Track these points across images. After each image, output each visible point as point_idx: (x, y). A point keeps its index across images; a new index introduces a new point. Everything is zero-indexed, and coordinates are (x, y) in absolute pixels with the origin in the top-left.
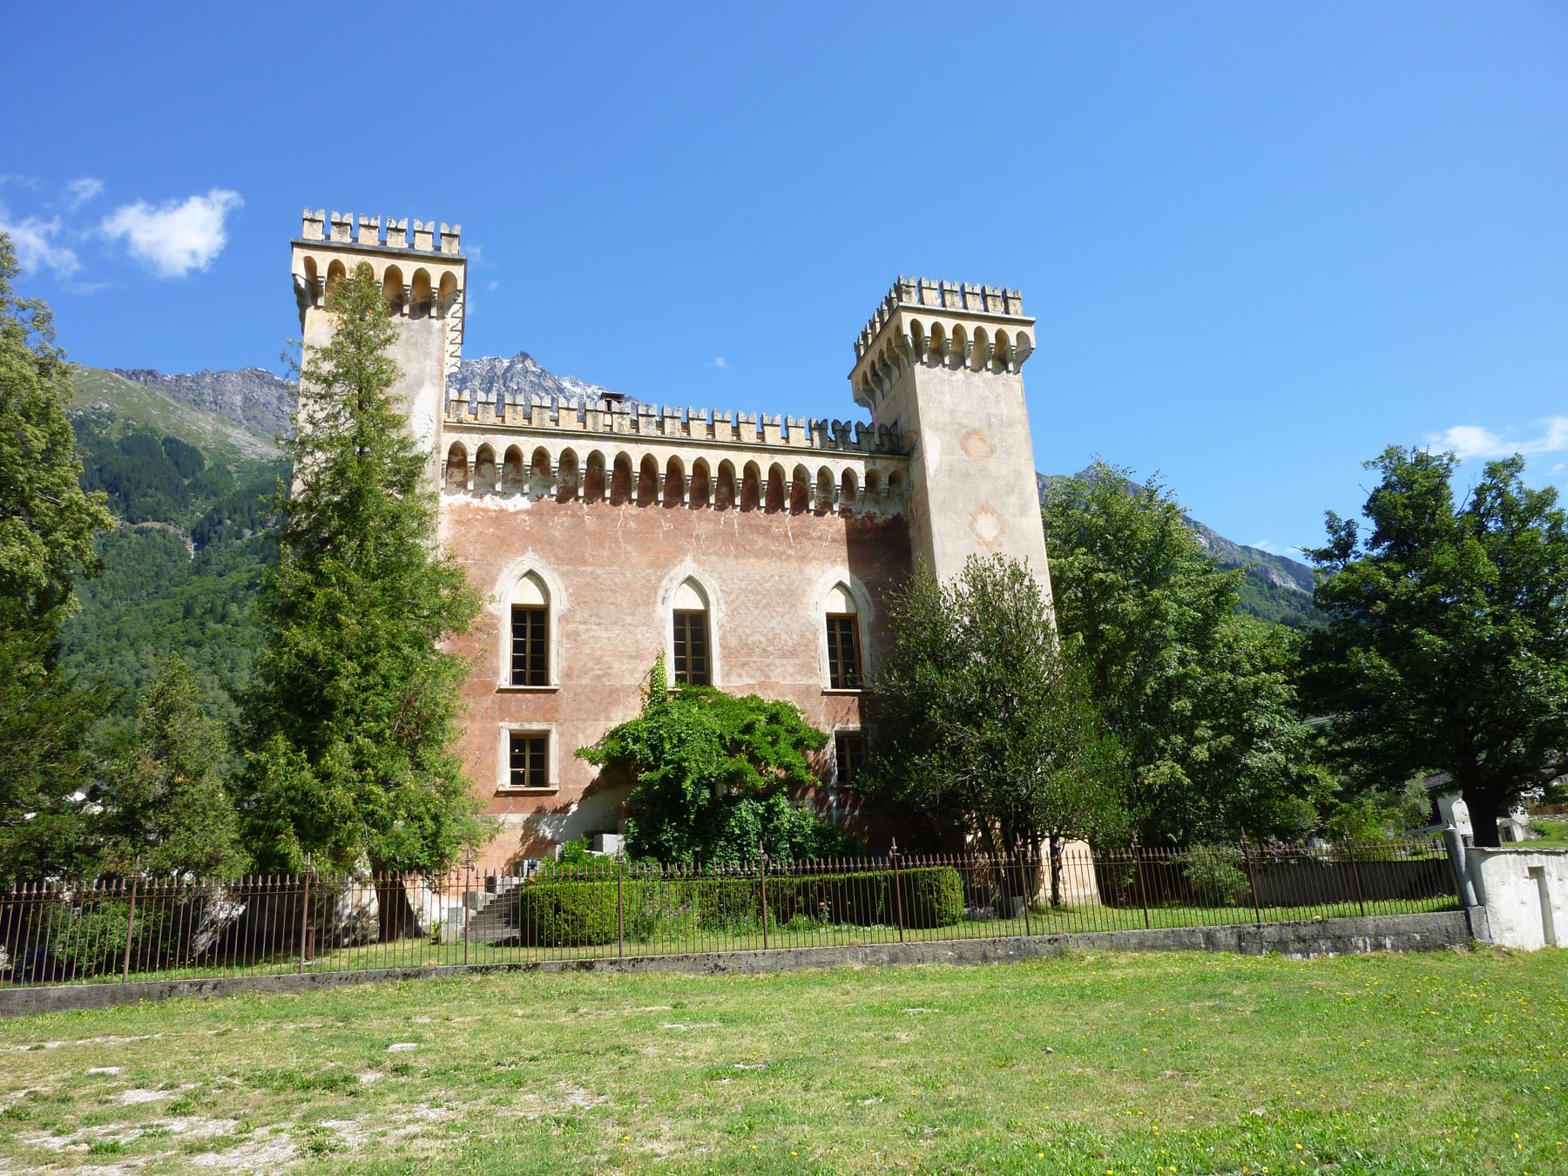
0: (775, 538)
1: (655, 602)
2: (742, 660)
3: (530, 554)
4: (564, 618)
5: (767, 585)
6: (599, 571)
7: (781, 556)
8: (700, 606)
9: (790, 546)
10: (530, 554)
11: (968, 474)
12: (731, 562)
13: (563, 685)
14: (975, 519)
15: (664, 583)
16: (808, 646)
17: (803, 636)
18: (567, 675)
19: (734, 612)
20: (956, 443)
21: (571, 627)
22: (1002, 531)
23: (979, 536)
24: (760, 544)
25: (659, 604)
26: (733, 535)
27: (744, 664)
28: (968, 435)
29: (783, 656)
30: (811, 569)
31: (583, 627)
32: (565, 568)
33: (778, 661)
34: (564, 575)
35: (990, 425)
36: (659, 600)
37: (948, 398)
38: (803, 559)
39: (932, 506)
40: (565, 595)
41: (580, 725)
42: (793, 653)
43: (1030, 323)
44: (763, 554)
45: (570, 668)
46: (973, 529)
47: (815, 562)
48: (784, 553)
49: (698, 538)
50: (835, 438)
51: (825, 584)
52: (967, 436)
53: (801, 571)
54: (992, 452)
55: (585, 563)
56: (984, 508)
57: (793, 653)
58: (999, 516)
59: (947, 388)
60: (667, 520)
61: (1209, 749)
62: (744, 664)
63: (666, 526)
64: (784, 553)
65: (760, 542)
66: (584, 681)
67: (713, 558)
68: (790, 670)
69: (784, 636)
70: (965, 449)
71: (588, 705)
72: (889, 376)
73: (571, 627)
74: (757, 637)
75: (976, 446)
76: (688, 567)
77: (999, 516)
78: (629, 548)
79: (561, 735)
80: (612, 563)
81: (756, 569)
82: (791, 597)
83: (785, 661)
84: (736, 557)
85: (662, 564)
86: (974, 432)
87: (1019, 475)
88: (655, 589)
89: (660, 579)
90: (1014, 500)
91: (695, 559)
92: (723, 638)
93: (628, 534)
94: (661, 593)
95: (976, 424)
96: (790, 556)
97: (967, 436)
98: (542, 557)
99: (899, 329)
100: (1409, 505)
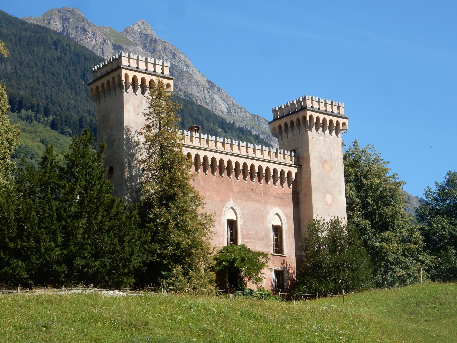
1: (222, 216)
5: (255, 212)
8: (235, 219)
9: (262, 198)
11: (324, 178)
14: (325, 195)
15: (224, 208)
17: (266, 233)
19: (245, 222)
22: (333, 201)
24: (253, 196)
25: (223, 216)
30: (269, 207)
33: (258, 241)
36: (223, 215)
37: (318, 146)
38: (266, 203)
39: (312, 189)
44: (254, 200)
46: (324, 199)
47: (270, 205)
48: (260, 200)
50: (367, 188)
51: (279, 214)
52: (324, 162)
53: (265, 208)
54: (331, 169)
56: (328, 191)
57: (262, 239)
58: (332, 195)
59: (318, 142)
61: (127, 295)
64: (260, 200)
67: (239, 200)
68: (262, 245)
70: (323, 167)
72: (292, 130)
74: (252, 232)
75: (327, 167)
76: (231, 203)
77: (332, 195)
82: (262, 218)
83: (260, 242)
84: (246, 201)
85: (224, 201)
87: (339, 179)
88: (222, 210)
89: (223, 207)
91: (234, 201)
92: (242, 231)
94: (223, 212)
95: (327, 158)
96: (262, 202)
97: (324, 162)
99: (120, 76)
100: (274, 111)
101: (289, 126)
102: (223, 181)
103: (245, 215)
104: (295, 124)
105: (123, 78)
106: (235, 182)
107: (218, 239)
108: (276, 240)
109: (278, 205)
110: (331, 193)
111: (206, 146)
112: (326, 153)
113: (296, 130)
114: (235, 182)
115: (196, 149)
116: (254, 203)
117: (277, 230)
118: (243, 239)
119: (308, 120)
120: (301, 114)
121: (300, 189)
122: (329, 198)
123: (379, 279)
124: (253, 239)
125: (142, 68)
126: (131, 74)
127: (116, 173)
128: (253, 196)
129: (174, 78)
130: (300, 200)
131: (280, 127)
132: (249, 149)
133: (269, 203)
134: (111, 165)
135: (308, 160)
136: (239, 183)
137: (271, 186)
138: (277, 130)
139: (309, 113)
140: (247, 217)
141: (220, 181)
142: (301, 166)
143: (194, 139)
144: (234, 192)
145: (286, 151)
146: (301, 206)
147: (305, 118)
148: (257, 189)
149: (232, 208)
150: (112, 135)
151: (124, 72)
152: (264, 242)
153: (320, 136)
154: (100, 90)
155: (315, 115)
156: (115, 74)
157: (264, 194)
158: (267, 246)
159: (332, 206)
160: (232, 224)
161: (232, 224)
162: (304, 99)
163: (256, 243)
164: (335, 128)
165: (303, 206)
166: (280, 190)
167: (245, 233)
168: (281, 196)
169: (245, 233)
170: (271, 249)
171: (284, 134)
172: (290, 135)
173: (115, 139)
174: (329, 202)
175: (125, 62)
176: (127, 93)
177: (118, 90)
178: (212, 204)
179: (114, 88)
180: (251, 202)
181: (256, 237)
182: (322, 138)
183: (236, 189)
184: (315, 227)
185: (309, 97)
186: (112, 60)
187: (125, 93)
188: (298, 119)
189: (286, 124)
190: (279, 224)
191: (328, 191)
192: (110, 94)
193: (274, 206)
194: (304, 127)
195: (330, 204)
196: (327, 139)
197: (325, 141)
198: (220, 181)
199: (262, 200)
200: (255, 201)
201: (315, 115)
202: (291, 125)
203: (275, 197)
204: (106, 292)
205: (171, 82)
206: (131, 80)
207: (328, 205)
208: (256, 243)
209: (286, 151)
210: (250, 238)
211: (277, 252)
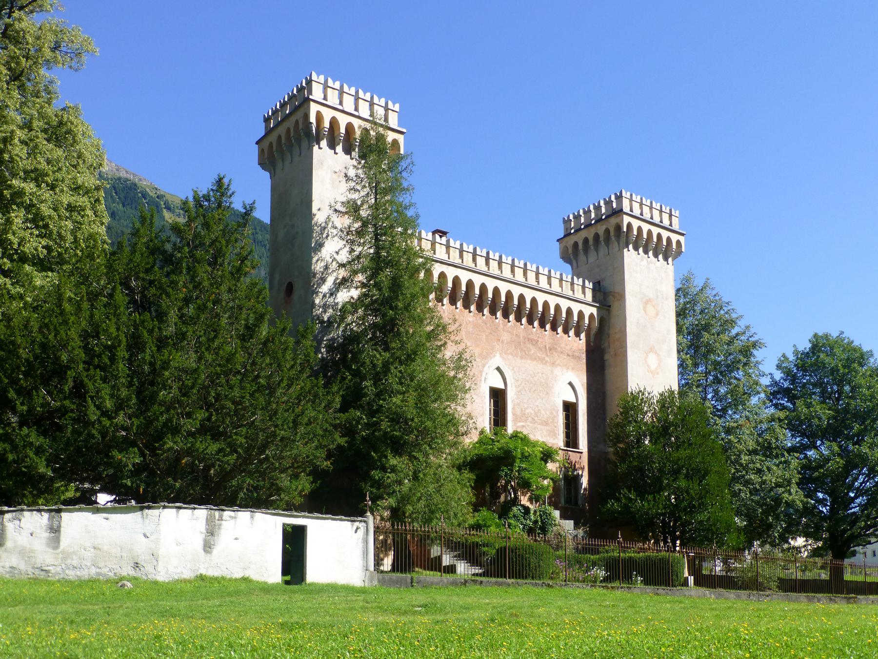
5: (536, 378)
7: (543, 361)
8: (575, 401)
15: (486, 369)
17: (551, 413)
19: (519, 393)
24: (533, 352)
29: (542, 424)
30: (557, 371)
33: (539, 426)
38: (553, 364)
43: (683, 235)
44: (534, 358)
46: (646, 362)
47: (559, 368)
48: (544, 359)
51: (569, 381)
54: (657, 315)
56: (651, 350)
57: (546, 423)
58: (658, 355)
67: (510, 357)
70: (645, 311)
77: (658, 355)
81: (531, 366)
82: (546, 388)
83: (542, 427)
84: (522, 358)
88: (481, 372)
89: (484, 366)
92: (513, 408)
96: (547, 362)
99: (307, 116)
101: (591, 242)
102: (484, 322)
103: (519, 383)
104: (601, 239)
105: (313, 119)
106: (505, 325)
107: (477, 412)
108: (567, 426)
110: (656, 353)
111: (458, 261)
112: (649, 289)
113: (603, 249)
114: (505, 325)
115: (441, 263)
116: (535, 363)
117: (570, 409)
118: (515, 420)
119: (625, 230)
120: (613, 221)
121: (606, 344)
122: (652, 360)
126: (328, 115)
127: (297, 292)
128: (533, 352)
129: (404, 130)
130: (607, 364)
131: (576, 244)
132: (529, 273)
133: (559, 365)
134: (289, 280)
135: (621, 296)
136: (511, 329)
137: (562, 337)
138: (570, 251)
139: (626, 219)
141: (480, 321)
142: (610, 306)
143: (437, 245)
144: (503, 342)
145: (587, 282)
146: (606, 371)
147: (619, 227)
148: (540, 340)
149: (498, 369)
150: (293, 226)
151: (314, 108)
152: (548, 428)
153: (642, 260)
154: (274, 149)
155: (636, 224)
156: (299, 114)
157: (550, 350)
158: (553, 434)
160: (498, 397)
161: (498, 397)
162: (619, 198)
163: (535, 428)
164: (664, 250)
165: (611, 374)
166: (576, 345)
167: (518, 412)
168: (577, 354)
169: (518, 412)
170: (558, 441)
171: (582, 257)
172: (592, 256)
173: (297, 233)
174: (653, 368)
175: (317, 93)
176: (320, 148)
177: (305, 143)
179: (299, 141)
180: (529, 361)
182: (645, 262)
183: (505, 337)
184: (633, 405)
185: (626, 194)
186: (295, 92)
187: (316, 148)
188: (607, 231)
189: (586, 241)
190: (573, 399)
192: (291, 155)
194: (616, 244)
195: (653, 367)
196: (652, 265)
198: (480, 321)
199: (547, 359)
201: (636, 224)
202: (596, 245)
203: (568, 355)
204: (232, 514)
205: (401, 138)
206: (327, 124)
207: (652, 372)
208: (535, 428)
209: (587, 282)
210: (526, 421)
211: (567, 444)
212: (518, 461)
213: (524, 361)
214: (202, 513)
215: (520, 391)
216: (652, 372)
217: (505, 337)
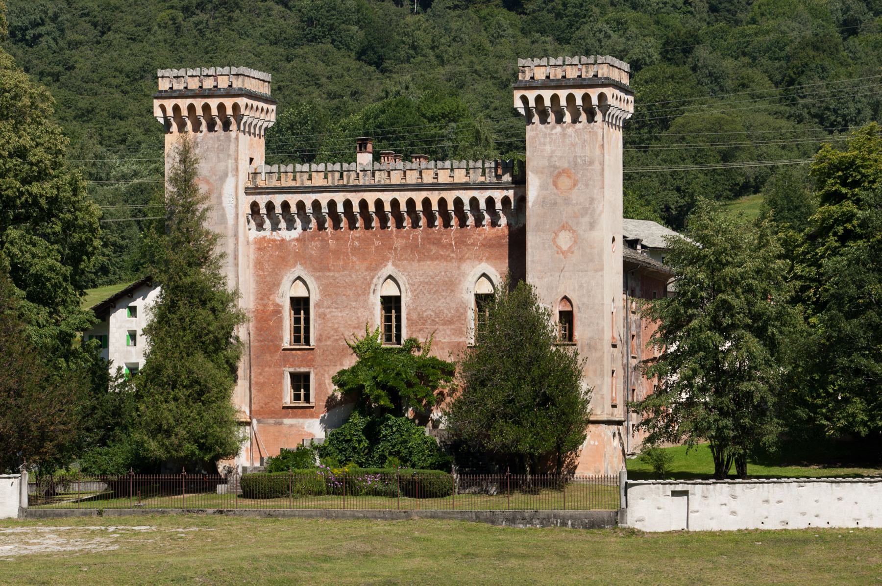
0: (444, 246)
2: (419, 327)
3: (299, 266)
4: (317, 305)
5: (437, 279)
6: (337, 275)
7: (447, 259)
9: (453, 252)
10: (299, 266)
11: (555, 204)
12: (415, 264)
13: (318, 346)
14: (557, 235)
15: (375, 280)
16: (460, 316)
17: (457, 311)
18: (319, 340)
19: (416, 297)
20: (550, 181)
21: (322, 310)
23: (560, 248)
24: (434, 251)
26: (417, 246)
27: (421, 330)
28: (559, 175)
29: (444, 324)
30: (466, 266)
31: (328, 310)
32: (318, 274)
33: (441, 327)
34: (317, 279)
35: (576, 164)
36: (372, 291)
38: (461, 259)
40: (318, 291)
41: (326, 368)
42: (450, 322)
44: (437, 257)
45: (321, 335)
48: (449, 256)
49: (396, 249)
53: (459, 268)
54: (575, 185)
55: (329, 270)
56: (564, 228)
57: (450, 322)
60: (377, 239)
62: (421, 330)
63: (377, 243)
64: (449, 256)
65: (434, 249)
66: (329, 343)
68: (448, 332)
69: (445, 311)
70: (555, 184)
71: (331, 357)
73: (322, 310)
74: (430, 312)
76: (389, 269)
77: (574, 232)
78: (355, 259)
79: (316, 374)
80: (344, 269)
81: (431, 268)
82: (451, 285)
83: (445, 327)
86: (564, 171)
88: (369, 284)
89: (372, 278)
90: (586, 220)
91: (393, 265)
92: (408, 314)
93: (354, 249)
94: (373, 287)
95: (566, 165)
96: (453, 258)
98: (305, 268)
105: (171, 163)
109: (488, 259)
123: (655, 536)
124: (430, 325)
125: (194, 87)
133: (468, 258)
140: (421, 287)
159: (572, 253)
160: (391, 304)
167: (414, 316)
169: (414, 316)
174: (565, 247)
178: (350, 276)
181: (437, 320)
183: (399, 243)
191: (563, 226)
193: (477, 263)
197: (564, 135)
200: (437, 258)
207: (563, 253)
210: (424, 324)
212: (609, 346)
213: (422, 263)
214: (694, 527)
215: (417, 295)
216: (563, 253)
217: (399, 243)
